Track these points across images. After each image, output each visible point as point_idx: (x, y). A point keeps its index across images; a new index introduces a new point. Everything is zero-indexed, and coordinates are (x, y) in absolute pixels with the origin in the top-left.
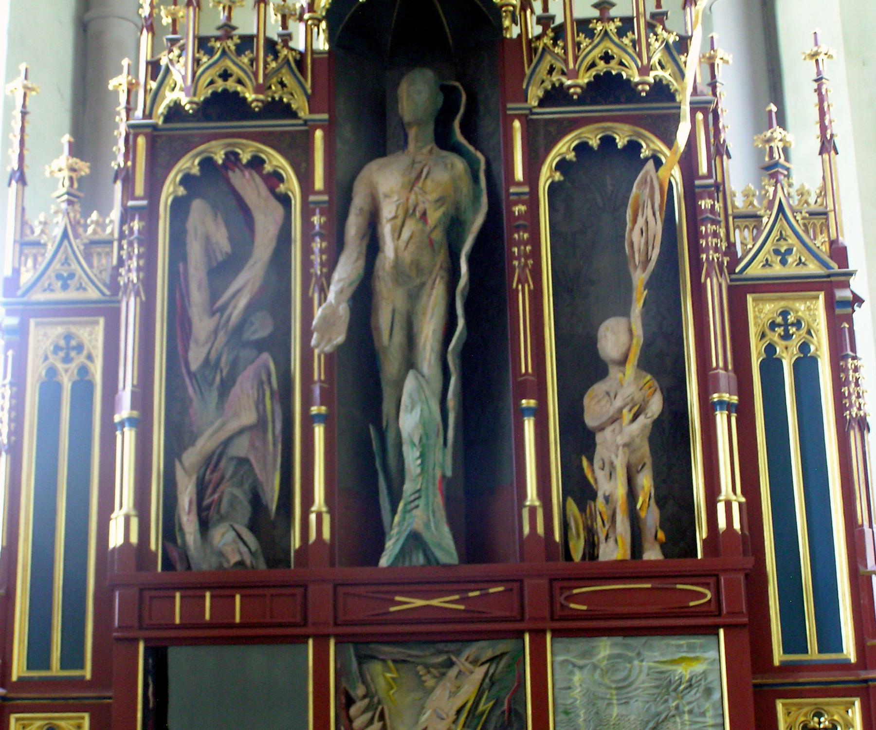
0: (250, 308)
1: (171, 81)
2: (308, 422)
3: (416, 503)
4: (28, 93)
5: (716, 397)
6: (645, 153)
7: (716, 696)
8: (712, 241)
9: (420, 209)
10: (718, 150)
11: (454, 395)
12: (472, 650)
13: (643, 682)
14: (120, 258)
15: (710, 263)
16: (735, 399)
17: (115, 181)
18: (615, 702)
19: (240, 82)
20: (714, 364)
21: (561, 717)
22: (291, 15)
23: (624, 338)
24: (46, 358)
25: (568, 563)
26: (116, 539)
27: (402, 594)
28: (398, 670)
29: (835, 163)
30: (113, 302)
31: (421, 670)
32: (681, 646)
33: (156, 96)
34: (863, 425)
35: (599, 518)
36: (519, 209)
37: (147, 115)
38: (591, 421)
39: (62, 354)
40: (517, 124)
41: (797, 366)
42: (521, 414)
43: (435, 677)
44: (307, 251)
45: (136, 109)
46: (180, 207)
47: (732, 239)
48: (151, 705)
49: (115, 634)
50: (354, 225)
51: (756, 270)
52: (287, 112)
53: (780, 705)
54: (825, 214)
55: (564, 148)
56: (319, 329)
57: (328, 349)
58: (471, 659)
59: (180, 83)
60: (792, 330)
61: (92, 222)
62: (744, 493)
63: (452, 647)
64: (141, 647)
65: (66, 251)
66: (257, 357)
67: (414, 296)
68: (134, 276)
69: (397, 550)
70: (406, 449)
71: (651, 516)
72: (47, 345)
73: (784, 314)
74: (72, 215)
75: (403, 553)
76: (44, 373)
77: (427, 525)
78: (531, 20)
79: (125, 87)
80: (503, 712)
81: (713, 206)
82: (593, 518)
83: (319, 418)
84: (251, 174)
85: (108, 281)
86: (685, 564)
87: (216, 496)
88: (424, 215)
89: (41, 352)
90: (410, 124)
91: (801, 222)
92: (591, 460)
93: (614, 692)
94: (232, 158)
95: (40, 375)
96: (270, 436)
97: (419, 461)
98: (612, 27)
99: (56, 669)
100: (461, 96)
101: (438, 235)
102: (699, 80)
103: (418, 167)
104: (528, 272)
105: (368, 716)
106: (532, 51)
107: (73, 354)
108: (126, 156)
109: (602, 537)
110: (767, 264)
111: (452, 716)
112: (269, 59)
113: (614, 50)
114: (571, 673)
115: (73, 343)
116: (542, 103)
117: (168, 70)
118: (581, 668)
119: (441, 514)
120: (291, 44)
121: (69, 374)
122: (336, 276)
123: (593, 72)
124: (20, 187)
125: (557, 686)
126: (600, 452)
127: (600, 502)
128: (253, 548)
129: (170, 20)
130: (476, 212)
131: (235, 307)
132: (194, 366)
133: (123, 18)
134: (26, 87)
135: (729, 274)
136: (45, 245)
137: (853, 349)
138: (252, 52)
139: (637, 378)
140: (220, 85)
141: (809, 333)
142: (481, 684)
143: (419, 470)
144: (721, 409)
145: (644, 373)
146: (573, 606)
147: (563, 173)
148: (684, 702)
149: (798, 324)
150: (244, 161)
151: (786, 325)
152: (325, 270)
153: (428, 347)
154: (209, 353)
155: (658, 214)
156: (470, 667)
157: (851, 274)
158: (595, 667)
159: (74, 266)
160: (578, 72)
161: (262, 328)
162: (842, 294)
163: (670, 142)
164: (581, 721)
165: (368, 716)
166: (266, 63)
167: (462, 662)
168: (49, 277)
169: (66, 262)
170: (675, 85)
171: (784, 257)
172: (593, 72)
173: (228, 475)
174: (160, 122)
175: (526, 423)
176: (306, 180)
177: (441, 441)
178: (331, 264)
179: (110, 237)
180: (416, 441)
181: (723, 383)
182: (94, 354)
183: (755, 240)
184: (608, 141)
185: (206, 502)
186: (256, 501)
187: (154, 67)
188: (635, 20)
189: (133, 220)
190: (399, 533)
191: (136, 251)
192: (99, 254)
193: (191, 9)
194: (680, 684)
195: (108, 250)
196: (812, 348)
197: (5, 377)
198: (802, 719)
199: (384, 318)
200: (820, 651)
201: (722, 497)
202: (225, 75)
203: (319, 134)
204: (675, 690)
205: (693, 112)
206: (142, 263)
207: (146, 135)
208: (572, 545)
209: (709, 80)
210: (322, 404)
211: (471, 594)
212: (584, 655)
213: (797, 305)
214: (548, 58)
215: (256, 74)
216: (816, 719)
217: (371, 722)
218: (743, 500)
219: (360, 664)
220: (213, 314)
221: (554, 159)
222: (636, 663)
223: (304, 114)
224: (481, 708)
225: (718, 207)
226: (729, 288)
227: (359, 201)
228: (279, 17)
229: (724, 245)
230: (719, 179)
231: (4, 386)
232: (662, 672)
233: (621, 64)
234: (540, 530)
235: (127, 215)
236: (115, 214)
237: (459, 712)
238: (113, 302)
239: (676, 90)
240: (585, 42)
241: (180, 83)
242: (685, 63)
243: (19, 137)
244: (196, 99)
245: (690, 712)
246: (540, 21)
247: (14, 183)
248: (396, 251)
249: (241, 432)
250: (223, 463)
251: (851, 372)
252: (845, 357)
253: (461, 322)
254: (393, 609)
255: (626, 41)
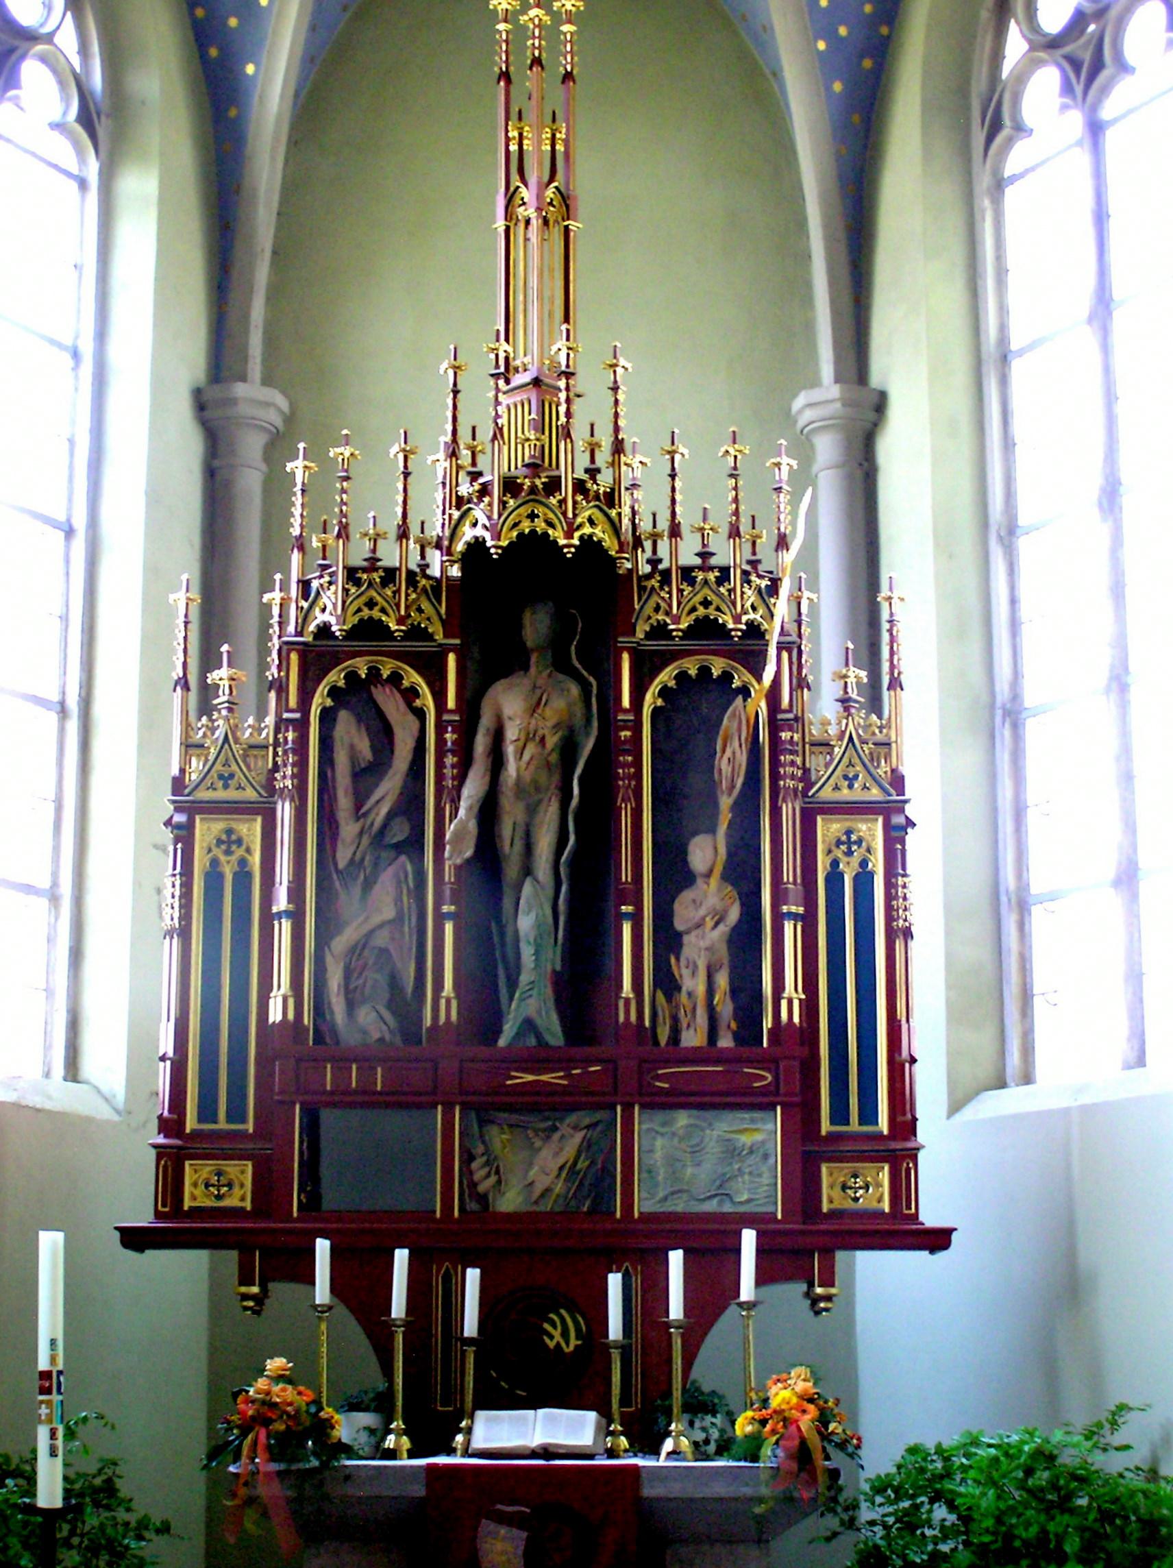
0: (390, 816)
1: (321, 604)
2: (440, 919)
3: (530, 993)
4: (190, 603)
5: (785, 909)
6: (736, 683)
7: (772, 1161)
8: (789, 770)
9: (540, 732)
10: (800, 683)
11: (565, 900)
12: (572, 1118)
13: (712, 1148)
14: (275, 763)
15: (787, 789)
16: (801, 910)
17: (270, 691)
18: (689, 1163)
19: (383, 610)
20: (785, 879)
21: (644, 1175)
22: (429, 544)
23: (709, 853)
24: (210, 850)
25: (654, 1048)
26: (275, 1015)
27: (517, 1071)
28: (512, 1133)
29: (900, 699)
30: (270, 803)
31: (530, 1133)
32: (744, 1119)
33: (306, 616)
34: (908, 934)
35: (682, 1010)
36: (625, 734)
37: (299, 633)
38: (679, 925)
39: (223, 847)
40: (626, 656)
41: (856, 879)
42: (620, 917)
43: (543, 1139)
44: (440, 765)
45: (288, 624)
46: (327, 717)
47: (808, 765)
48: (305, 1158)
49: (276, 1098)
50: (481, 744)
51: (827, 794)
52: (427, 636)
53: (824, 1169)
54: (889, 744)
55: (666, 676)
56: (451, 842)
57: (459, 861)
58: (572, 1125)
59: (330, 607)
60: (854, 848)
61: (249, 726)
62: (804, 992)
63: (558, 1115)
64: (298, 1107)
65: (226, 754)
66: (396, 859)
67: (532, 810)
68: (289, 783)
69: (513, 1034)
70: (523, 945)
71: (725, 1009)
72: (211, 839)
73: (849, 833)
74: (231, 721)
75: (518, 1035)
76: (208, 864)
77: (539, 1012)
78: (642, 557)
79: (278, 601)
80: (597, 1170)
81: (792, 737)
82: (677, 1007)
83: (449, 916)
84: (391, 690)
85: (264, 781)
86: (745, 1052)
87: (361, 981)
88: (543, 740)
89: (205, 845)
90: (532, 650)
91: (867, 752)
92: (678, 959)
93: (688, 1155)
94: (374, 672)
95: (205, 865)
96: (406, 929)
97: (534, 958)
98: (712, 576)
99: (222, 1125)
100: (578, 624)
101: (554, 758)
102: (786, 620)
103: (538, 692)
104: (630, 792)
105: (486, 1170)
106: (642, 589)
107: (234, 847)
108: (279, 667)
109: (685, 1025)
110: (837, 788)
111: (555, 1173)
112: (409, 591)
113: (711, 597)
114: (654, 1139)
115: (234, 837)
116: (649, 636)
117: (318, 593)
118: (662, 1135)
119: (551, 1004)
120: (428, 572)
121: (231, 864)
122: (466, 792)
123: (693, 616)
124: (185, 693)
125: (643, 1149)
126: (687, 951)
127: (683, 997)
128: (392, 1027)
129: (320, 545)
130: (588, 735)
131: (377, 814)
132: (342, 864)
133: (250, 467)
134: (188, 599)
135: (803, 796)
136: (209, 748)
137: (904, 868)
138: (395, 586)
139: (719, 890)
140: (366, 613)
141: (869, 851)
142: (580, 1146)
143: (532, 965)
144: (789, 919)
145: (726, 884)
146: (658, 1084)
147: (664, 700)
148: (745, 1165)
149: (859, 842)
150: (385, 676)
151: (849, 842)
152: (455, 783)
153: (544, 858)
154: (355, 853)
155: (744, 746)
156: (572, 1131)
157: (906, 802)
158: (674, 1134)
159: (234, 767)
160: (680, 618)
161: (400, 832)
162: (898, 820)
163: (759, 679)
164: (660, 1178)
165: (486, 1170)
166: (407, 595)
167: (564, 1128)
168: (212, 777)
169: (226, 764)
170: (765, 626)
171: (850, 781)
172: (693, 616)
173: (371, 962)
174: (310, 639)
175: (625, 926)
176: (439, 697)
177: (552, 941)
178: (461, 778)
179: (264, 743)
180: (532, 940)
181: (791, 897)
182: (252, 847)
183: (827, 765)
184: (705, 671)
185: (352, 986)
186: (394, 983)
187: (305, 585)
188: (732, 570)
189: (287, 731)
190: (515, 1018)
191: (291, 760)
192: (255, 756)
193: (341, 541)
194: (743, 1150)
195: (263, 753)
196: (870, 865)
197: (174, 869)
198: (842, 1179)
199: (507, 829)
200: (860, 1124)
201: (785, 995)
202: (371, 604)
203: (452, 658)
204: (739, 1154)
205: (780, 648)
206: (295, 770)
207: (298, 651)
208: (659, 1030)
209: (795, 617)
210: (452, 904)
211: (574, 1072)
212: (664, 1124)
213: (860, 826)
214: (655, 598)
215: (398, 605)
216: (853, 1180)
217: (488, 1175)
218: (803, 997)
219: (480, 1127)
220: (358, 819)
221: (656, 687)
222: (708, 1132)
223: (439, 637)
224: (579, 1166)
225: (796, 737)
226: (803, 810)
227: (486, 723)
228: (418, 547)
229: (800, 773)
230: (800, 715)
231: (174, 875)
232: (728, 1140)
233: (718, 609)
234: (633, 1017)
235: (280, 725)
236: (270, 720)
237: (561, 1168)
238: (270, 803)
239: (766, 630)
240: (688, 590)
241: (330, 607)
242: (775, 604)
243: (182, 646)
244: (345, 628)
245: (750, 1173)
246: (649, 561)
247: (178, 689)
248: (518, 770)
249: (381, 926)
250: (366, 953)
251: (900, 889)
252: (896, 875)
253: (572, 839)
254: (509, 1082)
255: (722, 590)
